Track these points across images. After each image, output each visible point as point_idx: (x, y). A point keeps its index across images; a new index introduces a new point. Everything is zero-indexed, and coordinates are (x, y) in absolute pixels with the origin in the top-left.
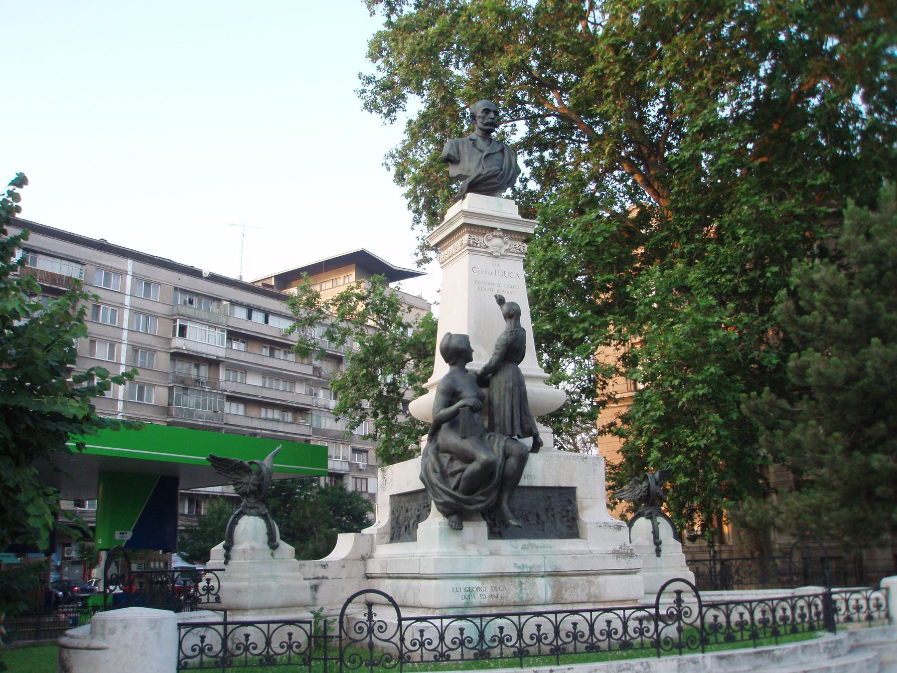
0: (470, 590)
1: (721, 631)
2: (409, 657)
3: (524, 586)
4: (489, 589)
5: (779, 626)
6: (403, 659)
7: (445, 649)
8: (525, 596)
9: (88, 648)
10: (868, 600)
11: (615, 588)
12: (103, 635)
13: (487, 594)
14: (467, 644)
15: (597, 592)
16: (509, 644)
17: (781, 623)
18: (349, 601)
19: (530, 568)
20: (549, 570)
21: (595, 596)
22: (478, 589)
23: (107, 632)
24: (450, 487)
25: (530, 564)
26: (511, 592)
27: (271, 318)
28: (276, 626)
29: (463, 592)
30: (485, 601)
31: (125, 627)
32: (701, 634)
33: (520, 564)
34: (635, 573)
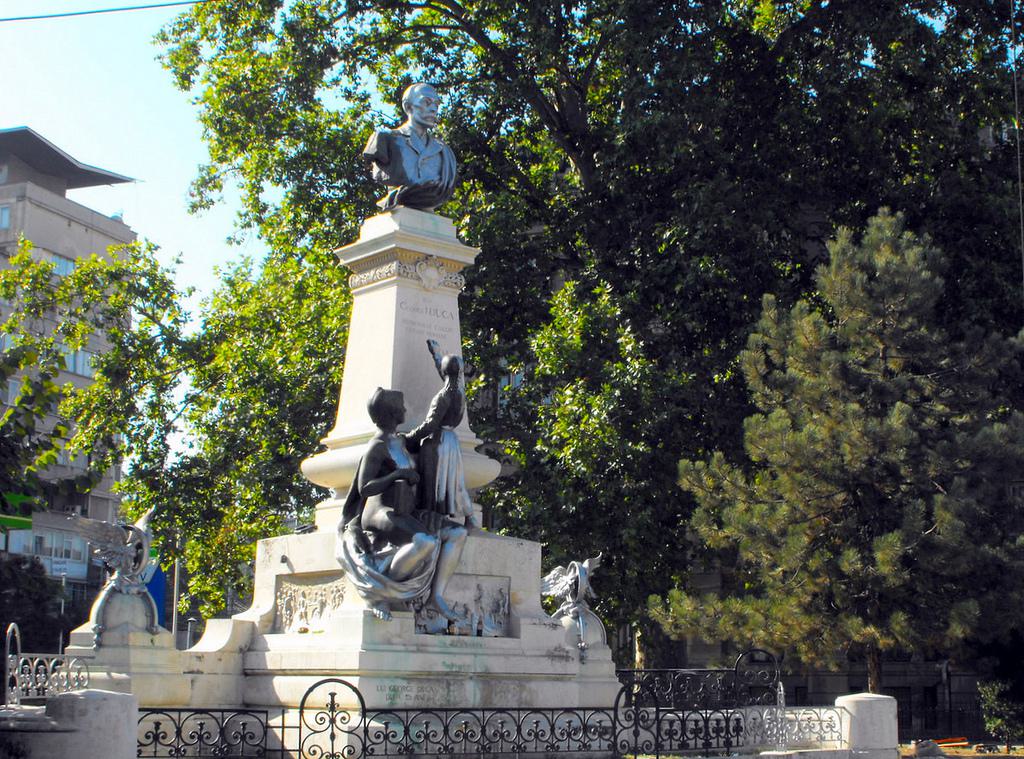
0: (395, 689)
1: (676, 737)
2: (372, 750)
3: (452, 688)
4: (415, 689)
5: (712, 738)
6: (520, 749)
7: (409, 743)
8: (452, 699)
9: (54, 731)
10: (683, 722)
11: (548, 695)
12: (72, 717)
13: (413, 694)
14: (247, 739)
15: (528, 698)
16: (251, 742)
17: (714, 735)
18: (311, 690)
19: (460, 667)
20: (479, 670)
21: (526, 703)
22: (404, 688)
23: (76, 713)
24: (377, 570)
25: (459, 663)
26: (438, 697)
27: (73, 224)
28: (188, 714)
29: (387, 691)
30: (411, 703)
31: (97, 709)
32: (657, 740)
33: (448, 663)
34: (570, 679)
